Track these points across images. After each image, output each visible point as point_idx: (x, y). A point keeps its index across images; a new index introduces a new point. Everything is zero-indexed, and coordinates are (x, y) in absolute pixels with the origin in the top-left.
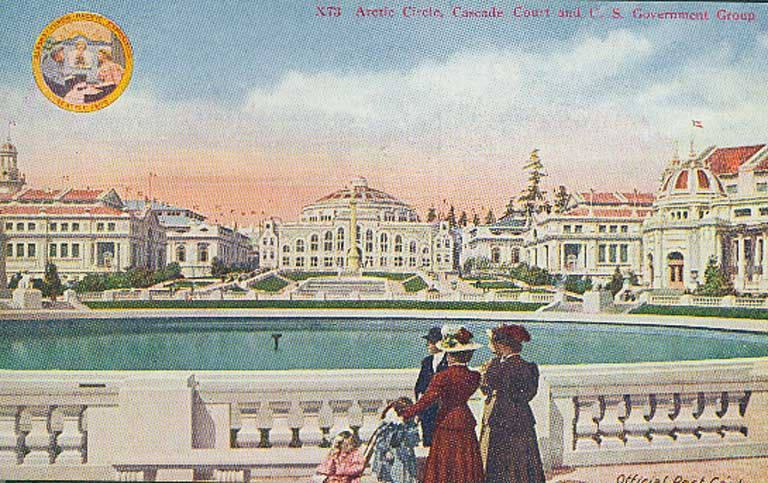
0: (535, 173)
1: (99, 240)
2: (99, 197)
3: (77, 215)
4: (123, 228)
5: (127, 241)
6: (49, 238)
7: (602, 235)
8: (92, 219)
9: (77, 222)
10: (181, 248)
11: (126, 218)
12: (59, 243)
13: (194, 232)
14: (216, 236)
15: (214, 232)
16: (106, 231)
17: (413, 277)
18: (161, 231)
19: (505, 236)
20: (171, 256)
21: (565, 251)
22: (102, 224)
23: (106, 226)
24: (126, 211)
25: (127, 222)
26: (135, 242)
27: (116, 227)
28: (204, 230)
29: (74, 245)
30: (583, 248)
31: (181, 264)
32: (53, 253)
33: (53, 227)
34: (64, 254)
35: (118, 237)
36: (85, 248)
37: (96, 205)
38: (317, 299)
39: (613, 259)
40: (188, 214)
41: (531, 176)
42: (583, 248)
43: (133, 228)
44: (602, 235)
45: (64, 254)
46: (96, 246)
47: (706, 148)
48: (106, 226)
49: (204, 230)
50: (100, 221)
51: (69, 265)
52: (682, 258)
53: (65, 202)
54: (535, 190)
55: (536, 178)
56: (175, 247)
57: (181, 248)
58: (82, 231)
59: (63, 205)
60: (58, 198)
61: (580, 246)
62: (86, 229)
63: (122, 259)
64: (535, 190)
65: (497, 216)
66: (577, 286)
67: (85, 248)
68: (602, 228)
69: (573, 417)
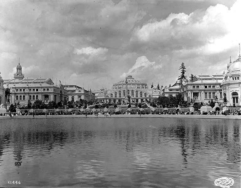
6: (15, 94)
13: (77, 92)
14: (83, 93)
15: (83, 92)
16: (46, 91)
20: (70, 100)
21: (193, 95)
28: (80, 91)
30: (199, 93)
34: (20, 99)
35: (49, 93)
40: (76, 86)
42: (199, 93)
44: (206, 89)
45: (20, 99)
47: (207, 75)
51: (22, 102)
54: (183, 77)
55: (183, 73)
56: (71, 97)
57: (73, 97)
58: (39, 91)
61: (199, 93)
64: (183, 77)
66: (197, 106)
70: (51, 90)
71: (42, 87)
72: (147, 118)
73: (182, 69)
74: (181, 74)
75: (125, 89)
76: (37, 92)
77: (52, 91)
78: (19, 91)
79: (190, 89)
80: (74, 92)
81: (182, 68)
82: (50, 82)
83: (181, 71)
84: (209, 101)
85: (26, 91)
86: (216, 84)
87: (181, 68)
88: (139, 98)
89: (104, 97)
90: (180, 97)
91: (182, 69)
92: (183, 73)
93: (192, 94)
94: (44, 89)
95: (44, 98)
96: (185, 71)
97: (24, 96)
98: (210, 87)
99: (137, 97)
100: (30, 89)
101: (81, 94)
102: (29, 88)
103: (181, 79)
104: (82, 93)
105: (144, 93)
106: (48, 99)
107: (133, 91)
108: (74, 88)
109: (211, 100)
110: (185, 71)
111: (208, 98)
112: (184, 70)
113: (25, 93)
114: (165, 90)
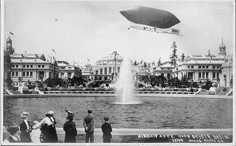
13: (67, 68)
14: (74, 69)
35: (45, 69)
36: (34, 74)
39: (106, 69)
40: (65, 62)
42: (194, 74)
54: (175, 55)
55: (175, 51)
64: (175, 55)
70: (47, 67)
71: (37, 63)
72: (85, 97)
73: (174, 48)
74: (173, 53)
75: (112, 66)
76: (43, 68)
77: (48, 68)
78: (41, 67)
79: (185, 69)
81: (174, 46)
82: (43, 58)
83: (172, 49)
84: (205, 81)
85: (34, 67)
86: (195, 65)
87: (173, 46)
88: (103, 75)
89: (89, 74)
90: (162, 76)
91: (174, 48)
92: (175, 51)
93: (187, 73)
95: (38, 75)
96: (177, 50)
97: (31, 73)
98: (28, 66)
99: (106, 74)
100: (24, 65)
102: (22, 63)
103: (172, 57)
104: (72, 69)
105: (135, 72)
106: (43, 76)
107: (110, 68)
108: (64, 65)
109: (206, 80)
110: (177, 50)
111: (205, 78)
113: (33, 69)
114: (156, 68)
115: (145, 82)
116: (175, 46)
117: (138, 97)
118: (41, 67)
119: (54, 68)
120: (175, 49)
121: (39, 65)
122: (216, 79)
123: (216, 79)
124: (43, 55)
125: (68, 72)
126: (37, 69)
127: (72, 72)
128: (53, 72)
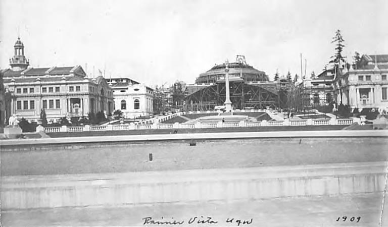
0: (340, 45)
1: (70, 97)
2: (71, 71)
3: (32, 83)
4: (85, 89)
5: (87, 97)
7: (44, 94)
8: (67, 84)
9: (58, 86)
10: (136, 101)
11: (86, 83)
12: (48, 99)
15: (143, 90)
17: (264, 114)
18: (110, 91)
19: (321, 85)
22: (73, 87)
23: (48, 89)
24: (87, 79)
25: (87, 85)
26: (92, 97)
27: (81, 88)
28: (136, 90)
29: (57, 100)
31: (123, 111)
32: (45, 106)
33: (44, 89)
34: (51, 106)
36: (63, 101)
37: (70, 76)
38: (108, 130)
41: (338, 47)
43: (90, 88)
45: (51, 106)
46: (358, 90)
48: (48, 89)
49: (136, 90)
50: (71, 86)
52: (125, 101)
53: (51, 75)
54: (339, 56)
55: (340, 49)
59: (26, 77)
60: (23, 73)
62: (38, 91)
63: (85, 109)
64: (339, 56)
65: (317, 75)
67: (63, 101)
68: (44, 89)
69: (128, 203)
73: (337, 42)
78: (75, 92)
80: (125, 91)
92: (340, 49)
94: (70, 87)
96: (343, 46)
97: (32, 102)
101: (140, 95)
106: (80, 107)
110: (343, 46)
112: (342, 43)
115: (164, 114)
116: (340, 39)
117: (341, 186)
118: (75, 92)
119: (102, 91)
120: (341, 43)
121: (70, 87)
122: (49, 118)
123: (49, 118)
124: (81, 68)
125: (134, 98)
126: (67, 95)
127: (217, 122)
128: (100, 99)
